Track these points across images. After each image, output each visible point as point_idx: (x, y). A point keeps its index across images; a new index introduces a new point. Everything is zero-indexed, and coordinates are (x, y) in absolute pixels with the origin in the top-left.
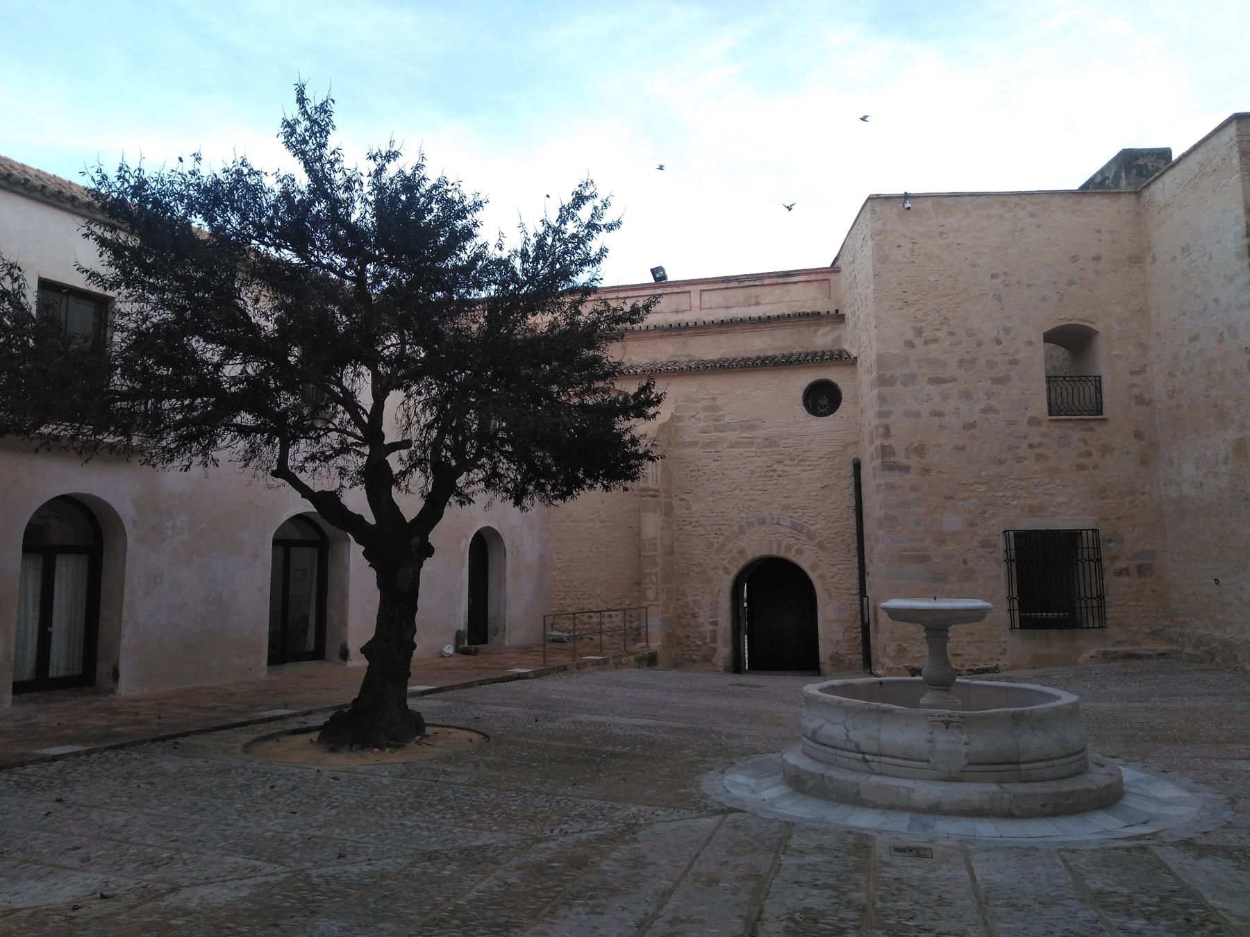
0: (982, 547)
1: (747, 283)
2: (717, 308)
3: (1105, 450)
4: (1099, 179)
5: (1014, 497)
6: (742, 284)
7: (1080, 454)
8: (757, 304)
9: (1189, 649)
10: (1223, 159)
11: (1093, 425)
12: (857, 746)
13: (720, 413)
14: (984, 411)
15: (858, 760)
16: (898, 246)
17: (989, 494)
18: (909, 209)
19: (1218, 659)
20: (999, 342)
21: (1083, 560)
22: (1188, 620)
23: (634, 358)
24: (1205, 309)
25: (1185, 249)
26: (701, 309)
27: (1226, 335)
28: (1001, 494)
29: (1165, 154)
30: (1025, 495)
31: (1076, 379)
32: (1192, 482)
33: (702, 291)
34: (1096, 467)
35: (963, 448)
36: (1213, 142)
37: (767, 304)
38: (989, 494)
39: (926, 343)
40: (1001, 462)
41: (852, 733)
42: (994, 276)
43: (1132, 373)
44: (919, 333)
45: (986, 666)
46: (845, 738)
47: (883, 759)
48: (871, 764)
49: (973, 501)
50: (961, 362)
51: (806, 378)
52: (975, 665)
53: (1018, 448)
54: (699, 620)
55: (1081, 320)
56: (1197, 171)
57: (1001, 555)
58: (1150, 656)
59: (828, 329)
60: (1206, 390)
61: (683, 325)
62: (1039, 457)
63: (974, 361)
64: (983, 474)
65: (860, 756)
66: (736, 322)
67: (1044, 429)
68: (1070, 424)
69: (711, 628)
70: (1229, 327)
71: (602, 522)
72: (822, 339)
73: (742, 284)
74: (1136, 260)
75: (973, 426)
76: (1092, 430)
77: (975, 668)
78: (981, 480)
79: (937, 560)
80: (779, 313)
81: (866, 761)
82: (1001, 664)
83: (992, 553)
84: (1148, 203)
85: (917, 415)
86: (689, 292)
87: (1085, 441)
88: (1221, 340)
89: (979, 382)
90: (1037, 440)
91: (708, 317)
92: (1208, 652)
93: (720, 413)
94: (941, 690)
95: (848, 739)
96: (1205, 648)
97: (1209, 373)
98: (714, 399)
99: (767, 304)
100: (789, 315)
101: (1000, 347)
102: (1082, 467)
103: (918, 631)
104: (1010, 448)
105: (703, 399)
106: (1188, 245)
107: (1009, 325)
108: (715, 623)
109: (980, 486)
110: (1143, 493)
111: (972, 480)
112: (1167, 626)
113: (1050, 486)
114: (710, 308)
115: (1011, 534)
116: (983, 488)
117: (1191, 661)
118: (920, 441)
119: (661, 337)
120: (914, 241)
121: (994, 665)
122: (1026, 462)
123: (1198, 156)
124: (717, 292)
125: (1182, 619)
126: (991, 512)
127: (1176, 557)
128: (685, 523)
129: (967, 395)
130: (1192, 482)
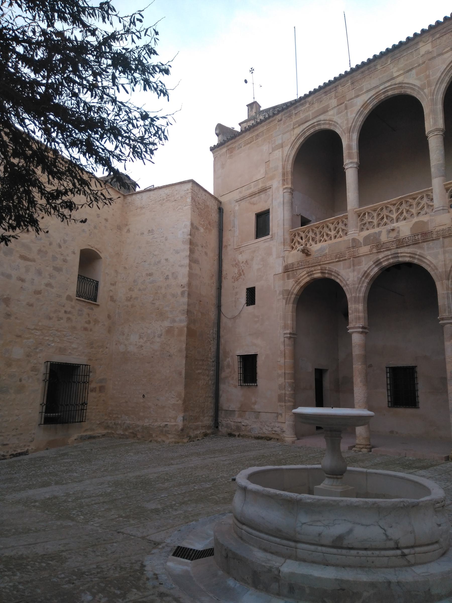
0: (32, 371)
3: (96, 321)
5: (53, 341)
7: (86, 322)
9: (120, 432)
10: (181, 197)
11: (93, 306)
12: (397, 543)
15: (396, 556)
17: (41, 337)
19: (139, 436)
20: (60, 246)
21: (77, 382)
22: (119, 416)
24: (159, 262)
25: (151, 232)
27: (170, 277)
28: (47, 338)
29: (135, 185)
30: (59, 341)
31: (89, 280)
32: (136, 345)
34: (91, 330)
35: (32, 305)
36: (177, 187)
38: (41, 337)
40: (50, 318)
41: (390, 532)
43: (111, 284)
45: (22, 451)
46: (384, 537)
47: (418, 550)
48: (409, 558)
49: (31, 340)
50: (40, 251)
52: (15, 451)
53: (59, 312)
55: (96, 249)
56: (165, 198)
57: (41, 377)
58: (99, 437)
60: (153, 301)
62: (69, 319)
63: (46, 253)
64: (40, 324)
65: (399, 552)
67: (73, 303)
68: (84, 304)
70: (173, 274)
74: (119, 228)
75: (39, 292)
76: (92, 309)
77: (15, 453)
78: (38, 328)
79: (4, 378)
81: (404, 555)
82: (30, 448)
83: (37, 375)
84: (129, 203)
85: (9, 276)
87: (89, 315)
88: (167, 278)
89: (47, 266)
90: (69, 309)
92: (133, 433)
94: (334, 478)
95: (388, 539)
96: (131, 431)
97: (157, 293)
101: (60, 250)
102: (86, 329)
104: (56, 311)
106: (153, 230)
107: (66, 239)
109: (37, 331)
110: (107, 348)
111: (33, 327)
112: (106, 420)
113: (70, 337)
115: (49, 363)
116: (39, 333)
117: (120, 438)
118: (8, 295)
121: (26, 449)
122: (62, 321)
123: (167, 191)
125: (114, 416)
126: (40, 349)
127: (116, 383)
129: (39, 273)
130: (136, 345)
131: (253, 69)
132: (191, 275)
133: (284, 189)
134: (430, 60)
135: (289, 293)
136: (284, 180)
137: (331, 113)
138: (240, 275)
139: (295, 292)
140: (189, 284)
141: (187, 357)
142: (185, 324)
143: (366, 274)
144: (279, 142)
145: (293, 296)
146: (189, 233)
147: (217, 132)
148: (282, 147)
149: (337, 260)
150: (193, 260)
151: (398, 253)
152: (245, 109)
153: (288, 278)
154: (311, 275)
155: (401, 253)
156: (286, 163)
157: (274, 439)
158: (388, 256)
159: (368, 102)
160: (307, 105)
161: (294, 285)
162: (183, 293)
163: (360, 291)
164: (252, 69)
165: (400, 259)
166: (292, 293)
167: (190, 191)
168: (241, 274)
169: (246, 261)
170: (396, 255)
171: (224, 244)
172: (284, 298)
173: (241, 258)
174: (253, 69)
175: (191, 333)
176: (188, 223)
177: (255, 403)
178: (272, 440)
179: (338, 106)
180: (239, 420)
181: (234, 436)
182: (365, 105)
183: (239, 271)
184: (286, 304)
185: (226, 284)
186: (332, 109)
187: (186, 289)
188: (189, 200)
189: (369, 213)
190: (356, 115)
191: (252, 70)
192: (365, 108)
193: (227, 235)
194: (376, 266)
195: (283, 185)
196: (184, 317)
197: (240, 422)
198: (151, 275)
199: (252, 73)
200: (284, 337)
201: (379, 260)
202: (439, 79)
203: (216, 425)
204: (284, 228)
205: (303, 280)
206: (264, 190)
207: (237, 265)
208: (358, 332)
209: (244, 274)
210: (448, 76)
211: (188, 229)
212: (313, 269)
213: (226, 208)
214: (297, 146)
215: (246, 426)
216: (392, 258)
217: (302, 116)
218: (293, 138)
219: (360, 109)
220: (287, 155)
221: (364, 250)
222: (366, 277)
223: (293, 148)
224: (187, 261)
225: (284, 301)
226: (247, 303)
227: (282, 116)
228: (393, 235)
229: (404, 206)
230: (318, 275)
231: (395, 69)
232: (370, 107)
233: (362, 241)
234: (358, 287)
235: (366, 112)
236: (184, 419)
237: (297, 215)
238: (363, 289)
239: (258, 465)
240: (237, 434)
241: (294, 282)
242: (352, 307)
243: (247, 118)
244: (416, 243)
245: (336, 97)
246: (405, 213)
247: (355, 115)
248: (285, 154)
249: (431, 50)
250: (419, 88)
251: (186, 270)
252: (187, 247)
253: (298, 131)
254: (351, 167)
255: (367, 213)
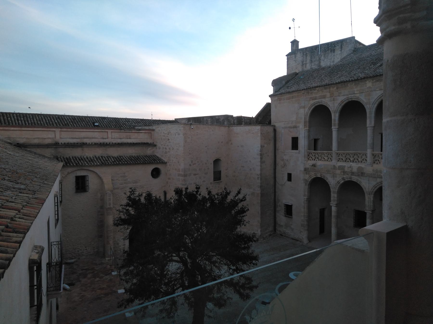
1: (127, 131)
2: (117, 138)
4: (217, 118)
6: (125, 131)
8: (130, 138)
13: (126, 178)
14: (203, 182)
16: (189, 138)
18: (192, 128)
23: (87, 154)
25: (242, 146)
26: (112, 138)
33: (112, 132)
37: (133, 138)
39: (193, 165)
42: (206, 147)
44: (192, 162)
51: (152, 167)
54: (119, 245)
55: (219, 157)
59: (151, 148)
61: (105, 143)
66: (123, 144)
69: (123, 246)
71: (83, 217)
72: (149, 151)
73: (125, 131)
76: (220, 184)
80: (137, 142)
86: (107, 132)
88: (251, 170)
91: (114, 141)
93: (126, 178)
98: (124, 173)
99: (133, 138)
100: (140, 143)
103: (50, 191)
105: (121, 173)
108: (124, 245)
114: (114, 138)
119: (97, 147)
120: (192, 136)
124: (116, 133)
128: (115, 215)
131: (294, 19)
132: (261, 170)
133: (305, 130)
134: (371, 91)
135: (305, 180)
136: (305, 125)
137: (327, 99)
138: (285, 166)
139: (309, 181)
140: (261, 174)
141: (261, 206)
142: (260, 192)
143: (338, 182)
144: (303, 105)
145: (308, 182)
146: (260, 150)
147: (273, 85)
148: (304, 108)
149: (327, 172)
150: (262, 162)
151: (351, 177)
152: (290, 45)
153: (306, 174)
154: (316, 175)
155: (353, 178)
156: (306, 116)
157: (299, 241)
158: (348, 177)
159: (344, 100)
160: (316, 91)
161: (308, 178)
162: (258, 178)
163: (336, 188)
164: (293, 19)
165: (352, 180)
166: (308, 181)
167: (260, 130)
168: (285, 165)
169: (287, 160)
170: (351, 178)
171: (277, 148)
172: (304, 182)
173: (286, 158)
174: (294, 19)
175: (262, 195)
176: (260, 146)
177: (291, 225)
178: (299, 241)
179: (330, 97)
180: (285, 230)
181: (283, 236)
182: (342, 102)
183: (284, 163)
184: (305, 185)
185: (278, 168)
186: (327, 98)
187: (259, 176)
188: (259, 134)
189: (341, 154)
190: (338, 105)
191: (293, 20)
192: (343, 103)
193: (278, 145)
194: (343, 180)
195: (305, 128)
196: (259, 189)
197: (285, 231)
198: (243, 167)
199: (294, 21)
200: (304, 200)
201: (344, 178)
202: (374, 102)
203: (275, 230)
204: (304, 149)
205: (313, 176)
206: (295, 127)
207: (283, 160)
208: (334, 206)
209: (286, 166)
210: (378, 102)
211: (259, 149)
212: (317, 173)
213: (278, 130)
214: (311, 109)
215: (288, 233)
216: (349, 178)
217: (314, 95)
218: (309, 105)
219: (340, 103)
220: (306, 113)
221: (338, 172)
222: (339, 184)
223: (310, 110)
224: (259, 164)
225: (304, 184)
226: (288, 180)
227: (304, 92)
228: (350, 169)
229: (356, 157)
230: (319, 176)
231: (356, 89)
232: (345, 103)
233: (337, 167)
234: (335, 187)
235: (343, 104)
236: (261, 231)
237: (312, 140)
238: (337, 188)
239: (324, 152)
240: (284, 235)
241: (309, 177)
242: (332, 195)
243: (290, 51)
244: (358, 176)
245: (329, 92)
246: (356, 160)
247: (337, 105)
248: (306, 112)
249: (371, 87)
250: (365, 103)
251: (259, 168)
252: (259, 157)
253: (312, 102)
254: (335, 131)
255: (341, 154)
